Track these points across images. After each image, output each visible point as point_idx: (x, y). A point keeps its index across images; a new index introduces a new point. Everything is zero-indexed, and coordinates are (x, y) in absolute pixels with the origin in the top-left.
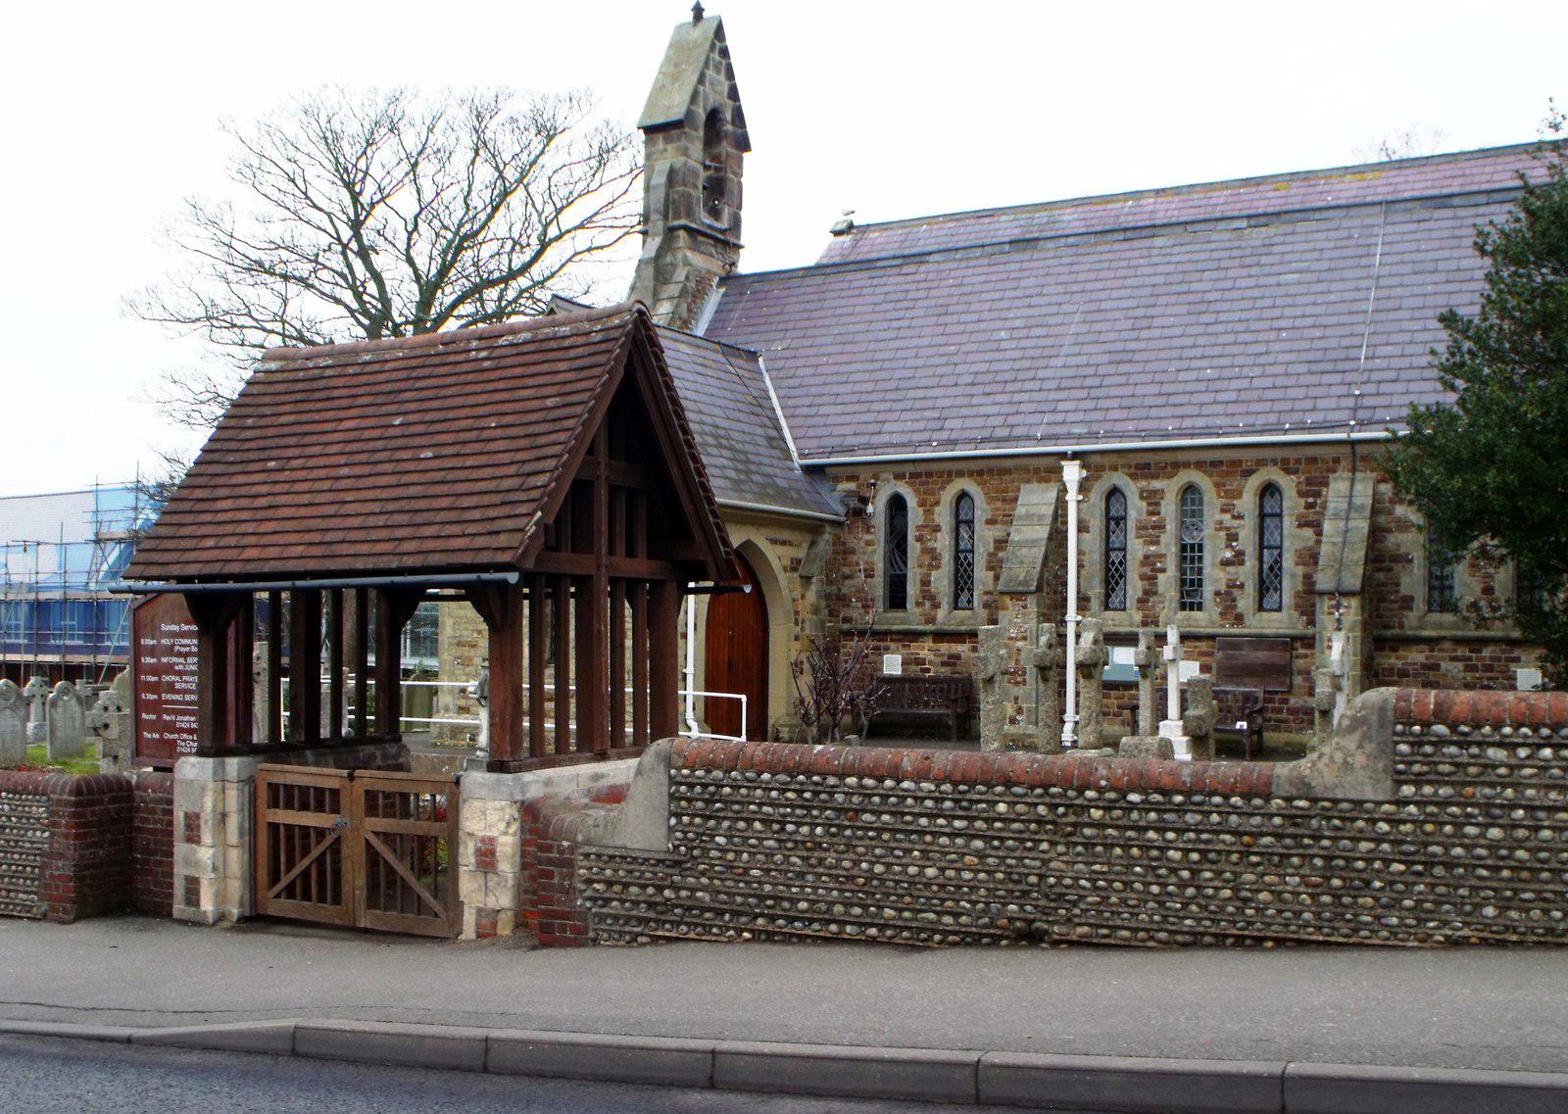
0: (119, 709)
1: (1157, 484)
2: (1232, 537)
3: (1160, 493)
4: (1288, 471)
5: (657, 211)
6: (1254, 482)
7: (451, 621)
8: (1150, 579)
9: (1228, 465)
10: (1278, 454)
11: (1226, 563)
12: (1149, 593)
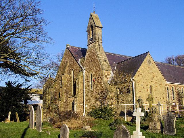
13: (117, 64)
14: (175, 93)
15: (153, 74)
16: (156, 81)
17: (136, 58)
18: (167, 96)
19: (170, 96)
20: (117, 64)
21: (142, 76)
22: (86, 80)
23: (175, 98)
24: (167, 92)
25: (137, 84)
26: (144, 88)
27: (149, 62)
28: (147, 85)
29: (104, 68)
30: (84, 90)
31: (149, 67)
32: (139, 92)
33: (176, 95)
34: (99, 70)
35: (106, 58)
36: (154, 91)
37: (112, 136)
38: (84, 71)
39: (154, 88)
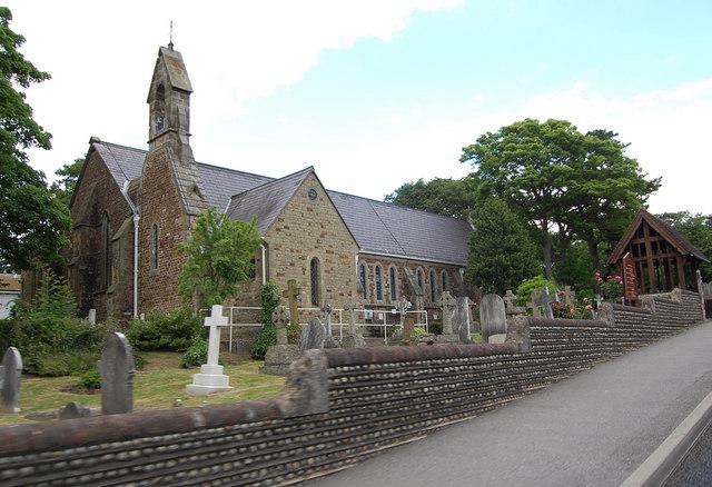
9: (385, 261)
14: (398, 282)
17: (242, 178)
19: (384, 291)
22: (140, 243)
25: (273, 254)
26: (292, 265)
28: (303, 258)
29: (191, 209)
30: (136, 270)
31: (310, 210)
33: (401, 287)
34: (176, 215)
36: (322, 274)
39: (322, 267)
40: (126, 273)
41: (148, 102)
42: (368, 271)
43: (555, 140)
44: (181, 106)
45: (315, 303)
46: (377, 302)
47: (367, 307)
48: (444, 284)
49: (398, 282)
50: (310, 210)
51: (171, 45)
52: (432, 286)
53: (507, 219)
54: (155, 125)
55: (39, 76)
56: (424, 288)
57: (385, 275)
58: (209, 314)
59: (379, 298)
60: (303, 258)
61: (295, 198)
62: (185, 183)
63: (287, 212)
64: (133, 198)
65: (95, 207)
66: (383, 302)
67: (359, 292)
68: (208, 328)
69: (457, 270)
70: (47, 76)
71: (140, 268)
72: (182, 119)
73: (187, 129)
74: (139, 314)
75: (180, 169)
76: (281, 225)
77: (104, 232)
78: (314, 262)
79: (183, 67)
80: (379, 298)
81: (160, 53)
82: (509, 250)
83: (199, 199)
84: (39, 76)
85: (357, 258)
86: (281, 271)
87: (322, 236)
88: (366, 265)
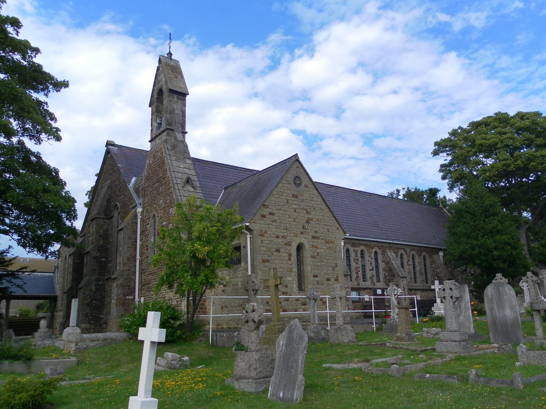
0: (247, 312)
1: (357, 249)
2: (371, 264)
3: (357, 251)
4: (379, 249)
5: (179, 124)
6: (374, 251)
7: (261, 272)
8: (357, 273)
9: (369, 245)
10: (380, 244)
11: (371, 270)
12: (357, 277)
13: (226, 188)
15: (307, 213)
16: (316, 232)
18: (360, 273)
19: (369, 274)
20: (226, 188)
21: (275, 218)
22: (142, 232)
23: (382, 279)
24: (360, 263)
25: (259, 240)
26: (278, 251)
27: (297, 182)
30: (138, 257)
31: (295, 196)
32: (264, 261)
33: (384, 270)
35: (193, 172)
37: (1, 198)
38: (139, 210)
39: (307, 252)
40: (129, 260)
41: (150, 106)
42: (353, 255)
43: (526, 129)
44: (177, 107)
45: (301, 288)
46: (363, 284)
47: (353, 289)
48: (425, 266)
49: (382, 265)
50: (295, 196)
51: (170, 54)
52: (414, 268)
53: (487, 202)
54: (155, 125)
55: (60, 85)
56: (407, 270)
57: (369, 258)
58: (143, 324)
59: (364, 279)
60: (289, 244)
61: (280, 185)
62: (180, 175)
63: (273, 199)
64: (137, 191)
65: (109, 201)
66: (368, 284)
67: (345, 275)
68: (142, 342)
69: (437, 253)
70: (65, 84)
71: (141, 254)
72: (178, 119)
73: (183, 126)
74: (140, 297)
75: (175, 163)
76: (266, 212)
77: (115, 223)
78: (300, 248)
79: (180, 73)
80: (364, 279)
81: (160, 62)
82: (492, 233)
83: (192, 190)
84: (60, 85)
85: (342, 244)
86: (266, 257)
87: (307, 222)
88: (352, 249)
